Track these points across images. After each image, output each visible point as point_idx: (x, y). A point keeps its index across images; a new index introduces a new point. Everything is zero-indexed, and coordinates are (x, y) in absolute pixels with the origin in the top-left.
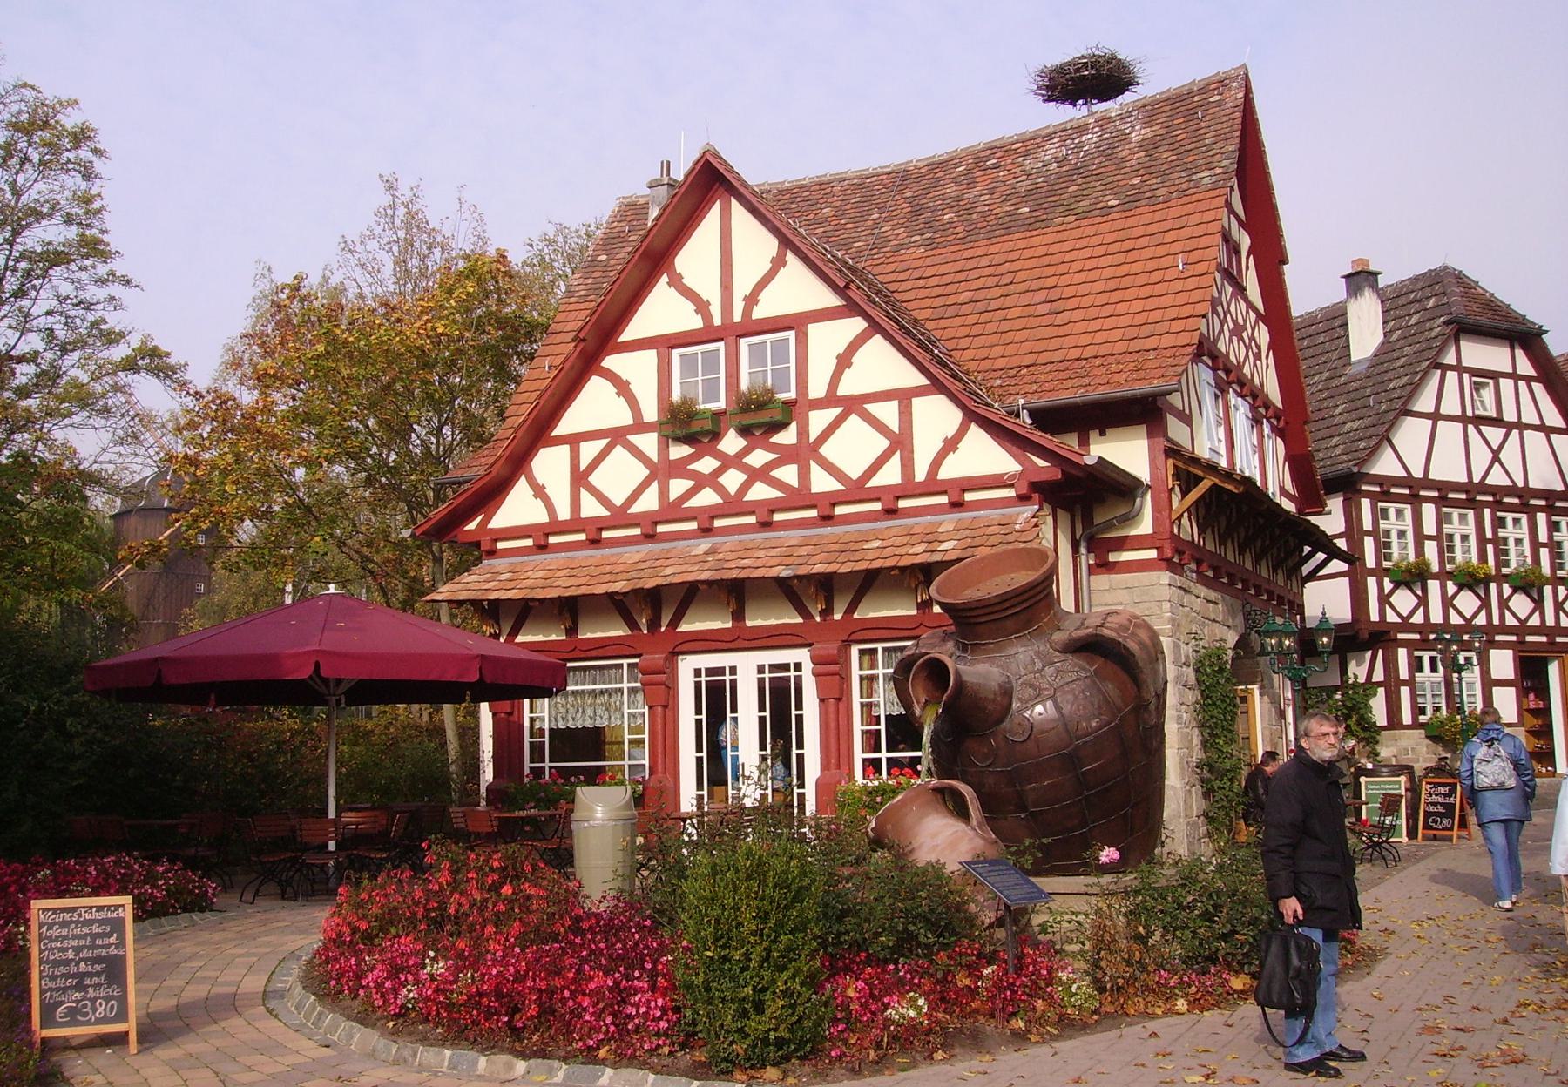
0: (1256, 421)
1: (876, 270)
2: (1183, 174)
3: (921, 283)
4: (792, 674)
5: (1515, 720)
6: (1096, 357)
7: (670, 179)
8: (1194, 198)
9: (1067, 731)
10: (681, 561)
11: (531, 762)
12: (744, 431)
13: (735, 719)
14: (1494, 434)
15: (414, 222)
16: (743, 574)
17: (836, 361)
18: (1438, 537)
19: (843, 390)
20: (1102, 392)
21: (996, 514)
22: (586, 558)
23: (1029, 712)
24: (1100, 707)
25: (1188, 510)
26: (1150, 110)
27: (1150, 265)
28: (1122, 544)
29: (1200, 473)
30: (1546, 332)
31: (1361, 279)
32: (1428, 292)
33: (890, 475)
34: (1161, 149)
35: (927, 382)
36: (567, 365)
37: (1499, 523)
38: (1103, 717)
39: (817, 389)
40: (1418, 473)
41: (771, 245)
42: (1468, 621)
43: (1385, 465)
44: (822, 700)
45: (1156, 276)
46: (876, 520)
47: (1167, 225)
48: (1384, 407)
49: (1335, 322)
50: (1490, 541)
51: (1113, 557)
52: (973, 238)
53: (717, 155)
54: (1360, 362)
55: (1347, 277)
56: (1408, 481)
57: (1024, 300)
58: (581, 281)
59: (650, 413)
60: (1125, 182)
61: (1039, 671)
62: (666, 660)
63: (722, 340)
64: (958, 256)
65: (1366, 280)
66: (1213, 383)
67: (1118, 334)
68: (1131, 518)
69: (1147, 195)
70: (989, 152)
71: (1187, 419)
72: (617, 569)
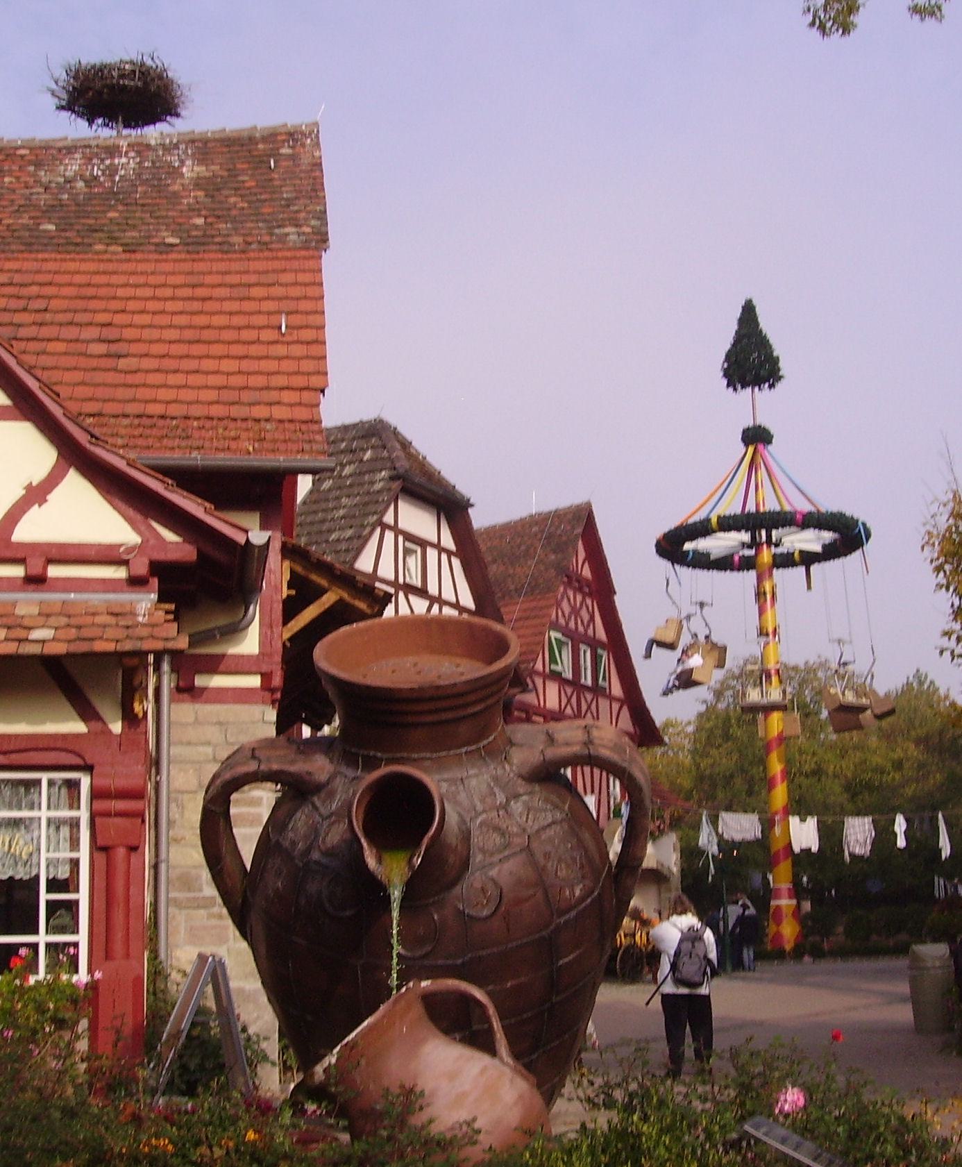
26: (203, 147)
28: (214, 665)
29: (324, 583)
30: (472, 505)
51: (200, 681)
61: (505, 807)
68: (235, 630)
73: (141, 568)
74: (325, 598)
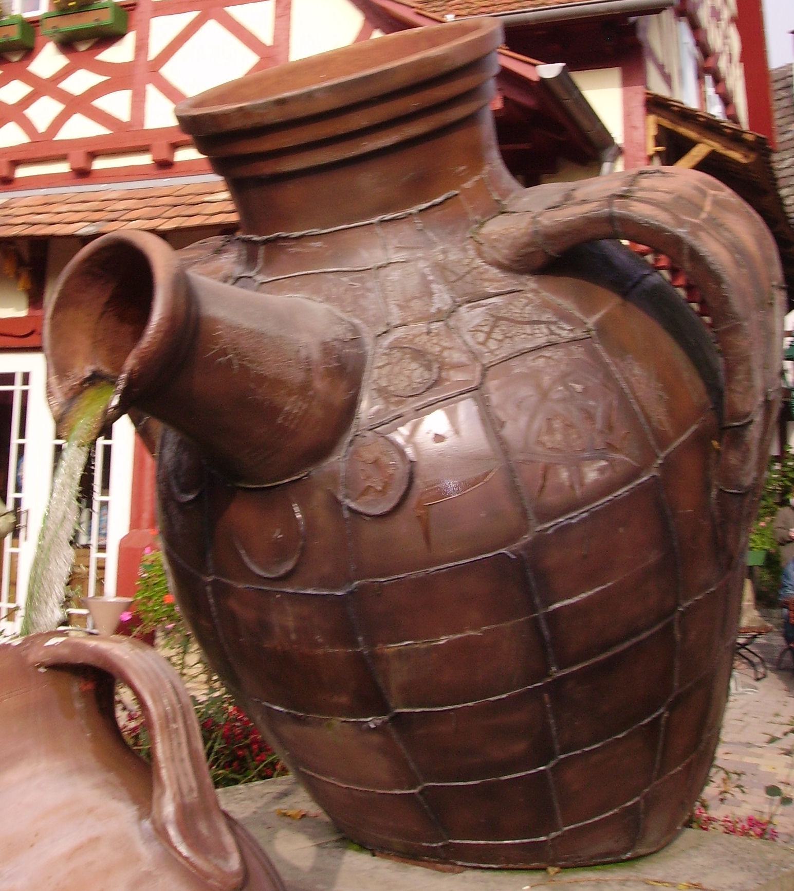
9: (514, 489)
12: (67, 44)
23: (404, 430)
24: (609, 427)
38: (617, 456)
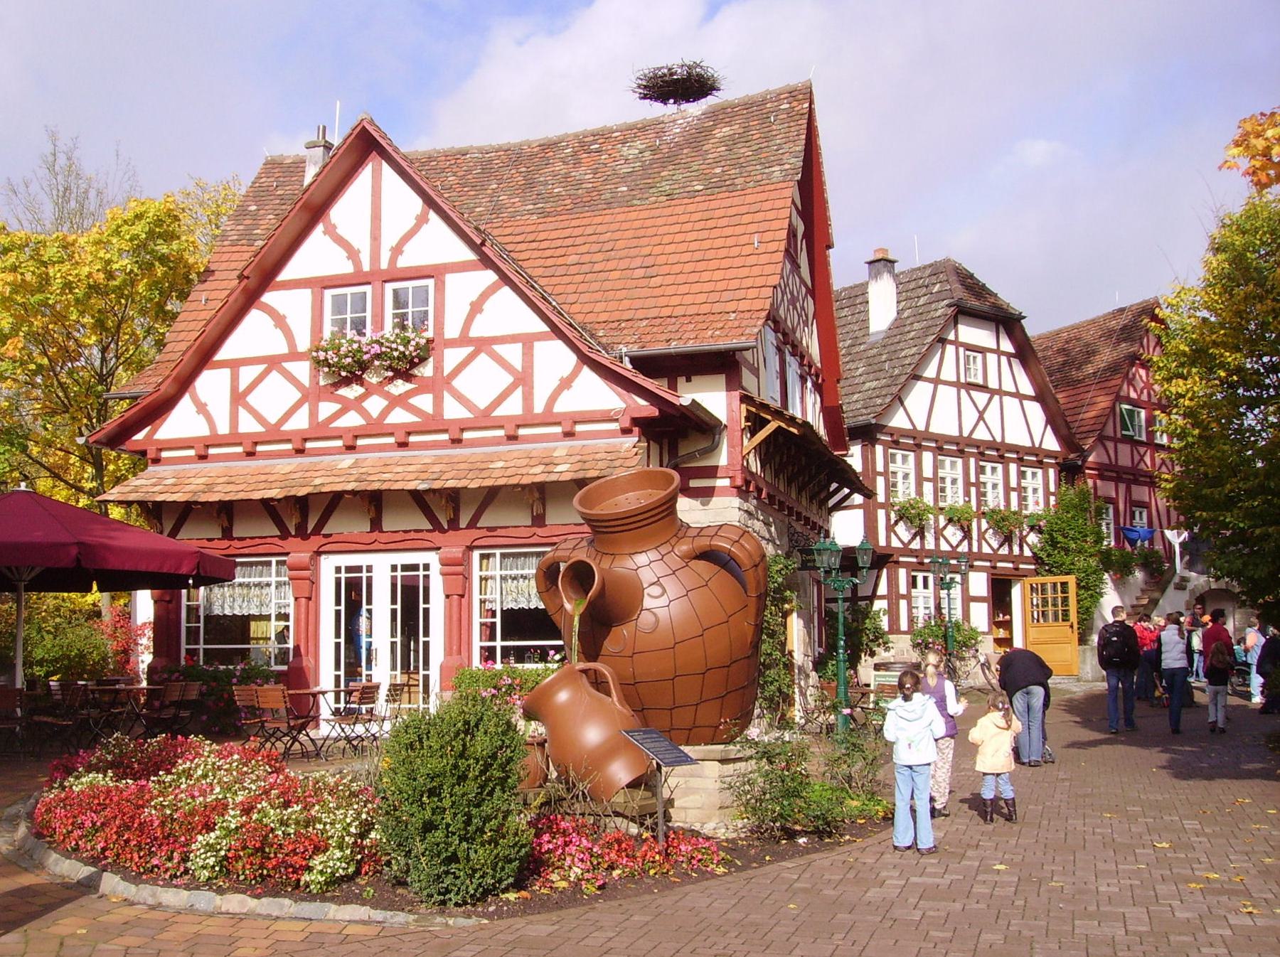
0: (803, 379)
1: (495, 232)
2: (758, 167)
3: (534, 245)
4: (421, 573)
5: (986, 629)
6: (684, 316)
7: (326, 142)
8: (767, 188)
10: (329, 473)
11: (187, 644)
13: (369, 611)
14: (982, 398)
15: (72, 170)
16: (385, 487)
17: (484, 307)
18: (935, 479)
19: (474, 333)
20: (691, 346)
21: (602, 443)
22: (243, 468)
25: (755, 448)
27: (730, 242)
29: (769, 417)
30: (1024, 317)
31: (882, 264)
32: (934, 279)
33: (513, 407)
34: (739, 145)
35: (548, 329)
36: (231, 299)
37: (981, 470)
39: (452, 331)
40: (921, 427)
41: (417, 203)
42: (954, 548)
43: (898, 421)
44: (447, 596)
45: (735, 251)
46: (499, 444)
47: (744, 209)
48: (897, 372)
49: (858, 295)
50: (973, 485)
52: (579, 210)
53: (372, 122)
54: (878, 333)
55: (870, 263)
56: (913, 434)
57: (623, 264)
58: (233, 227)
59: (304, 344)
60: (708, 171)
62: (311, 558)
63: (370, 283)
64: (566, 224)
65: (885, 266)
66: (775, 342)
67: (702, 298)
69: (728, 183)
70: (592, 138)
71: (755, 372)
72: (271, 478)
73: (627, 424)
74: (768, 426)
